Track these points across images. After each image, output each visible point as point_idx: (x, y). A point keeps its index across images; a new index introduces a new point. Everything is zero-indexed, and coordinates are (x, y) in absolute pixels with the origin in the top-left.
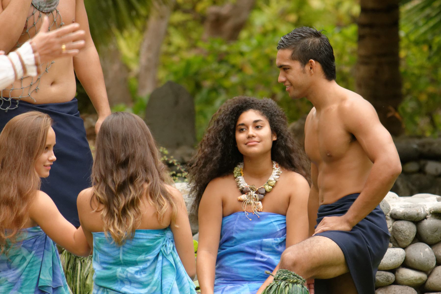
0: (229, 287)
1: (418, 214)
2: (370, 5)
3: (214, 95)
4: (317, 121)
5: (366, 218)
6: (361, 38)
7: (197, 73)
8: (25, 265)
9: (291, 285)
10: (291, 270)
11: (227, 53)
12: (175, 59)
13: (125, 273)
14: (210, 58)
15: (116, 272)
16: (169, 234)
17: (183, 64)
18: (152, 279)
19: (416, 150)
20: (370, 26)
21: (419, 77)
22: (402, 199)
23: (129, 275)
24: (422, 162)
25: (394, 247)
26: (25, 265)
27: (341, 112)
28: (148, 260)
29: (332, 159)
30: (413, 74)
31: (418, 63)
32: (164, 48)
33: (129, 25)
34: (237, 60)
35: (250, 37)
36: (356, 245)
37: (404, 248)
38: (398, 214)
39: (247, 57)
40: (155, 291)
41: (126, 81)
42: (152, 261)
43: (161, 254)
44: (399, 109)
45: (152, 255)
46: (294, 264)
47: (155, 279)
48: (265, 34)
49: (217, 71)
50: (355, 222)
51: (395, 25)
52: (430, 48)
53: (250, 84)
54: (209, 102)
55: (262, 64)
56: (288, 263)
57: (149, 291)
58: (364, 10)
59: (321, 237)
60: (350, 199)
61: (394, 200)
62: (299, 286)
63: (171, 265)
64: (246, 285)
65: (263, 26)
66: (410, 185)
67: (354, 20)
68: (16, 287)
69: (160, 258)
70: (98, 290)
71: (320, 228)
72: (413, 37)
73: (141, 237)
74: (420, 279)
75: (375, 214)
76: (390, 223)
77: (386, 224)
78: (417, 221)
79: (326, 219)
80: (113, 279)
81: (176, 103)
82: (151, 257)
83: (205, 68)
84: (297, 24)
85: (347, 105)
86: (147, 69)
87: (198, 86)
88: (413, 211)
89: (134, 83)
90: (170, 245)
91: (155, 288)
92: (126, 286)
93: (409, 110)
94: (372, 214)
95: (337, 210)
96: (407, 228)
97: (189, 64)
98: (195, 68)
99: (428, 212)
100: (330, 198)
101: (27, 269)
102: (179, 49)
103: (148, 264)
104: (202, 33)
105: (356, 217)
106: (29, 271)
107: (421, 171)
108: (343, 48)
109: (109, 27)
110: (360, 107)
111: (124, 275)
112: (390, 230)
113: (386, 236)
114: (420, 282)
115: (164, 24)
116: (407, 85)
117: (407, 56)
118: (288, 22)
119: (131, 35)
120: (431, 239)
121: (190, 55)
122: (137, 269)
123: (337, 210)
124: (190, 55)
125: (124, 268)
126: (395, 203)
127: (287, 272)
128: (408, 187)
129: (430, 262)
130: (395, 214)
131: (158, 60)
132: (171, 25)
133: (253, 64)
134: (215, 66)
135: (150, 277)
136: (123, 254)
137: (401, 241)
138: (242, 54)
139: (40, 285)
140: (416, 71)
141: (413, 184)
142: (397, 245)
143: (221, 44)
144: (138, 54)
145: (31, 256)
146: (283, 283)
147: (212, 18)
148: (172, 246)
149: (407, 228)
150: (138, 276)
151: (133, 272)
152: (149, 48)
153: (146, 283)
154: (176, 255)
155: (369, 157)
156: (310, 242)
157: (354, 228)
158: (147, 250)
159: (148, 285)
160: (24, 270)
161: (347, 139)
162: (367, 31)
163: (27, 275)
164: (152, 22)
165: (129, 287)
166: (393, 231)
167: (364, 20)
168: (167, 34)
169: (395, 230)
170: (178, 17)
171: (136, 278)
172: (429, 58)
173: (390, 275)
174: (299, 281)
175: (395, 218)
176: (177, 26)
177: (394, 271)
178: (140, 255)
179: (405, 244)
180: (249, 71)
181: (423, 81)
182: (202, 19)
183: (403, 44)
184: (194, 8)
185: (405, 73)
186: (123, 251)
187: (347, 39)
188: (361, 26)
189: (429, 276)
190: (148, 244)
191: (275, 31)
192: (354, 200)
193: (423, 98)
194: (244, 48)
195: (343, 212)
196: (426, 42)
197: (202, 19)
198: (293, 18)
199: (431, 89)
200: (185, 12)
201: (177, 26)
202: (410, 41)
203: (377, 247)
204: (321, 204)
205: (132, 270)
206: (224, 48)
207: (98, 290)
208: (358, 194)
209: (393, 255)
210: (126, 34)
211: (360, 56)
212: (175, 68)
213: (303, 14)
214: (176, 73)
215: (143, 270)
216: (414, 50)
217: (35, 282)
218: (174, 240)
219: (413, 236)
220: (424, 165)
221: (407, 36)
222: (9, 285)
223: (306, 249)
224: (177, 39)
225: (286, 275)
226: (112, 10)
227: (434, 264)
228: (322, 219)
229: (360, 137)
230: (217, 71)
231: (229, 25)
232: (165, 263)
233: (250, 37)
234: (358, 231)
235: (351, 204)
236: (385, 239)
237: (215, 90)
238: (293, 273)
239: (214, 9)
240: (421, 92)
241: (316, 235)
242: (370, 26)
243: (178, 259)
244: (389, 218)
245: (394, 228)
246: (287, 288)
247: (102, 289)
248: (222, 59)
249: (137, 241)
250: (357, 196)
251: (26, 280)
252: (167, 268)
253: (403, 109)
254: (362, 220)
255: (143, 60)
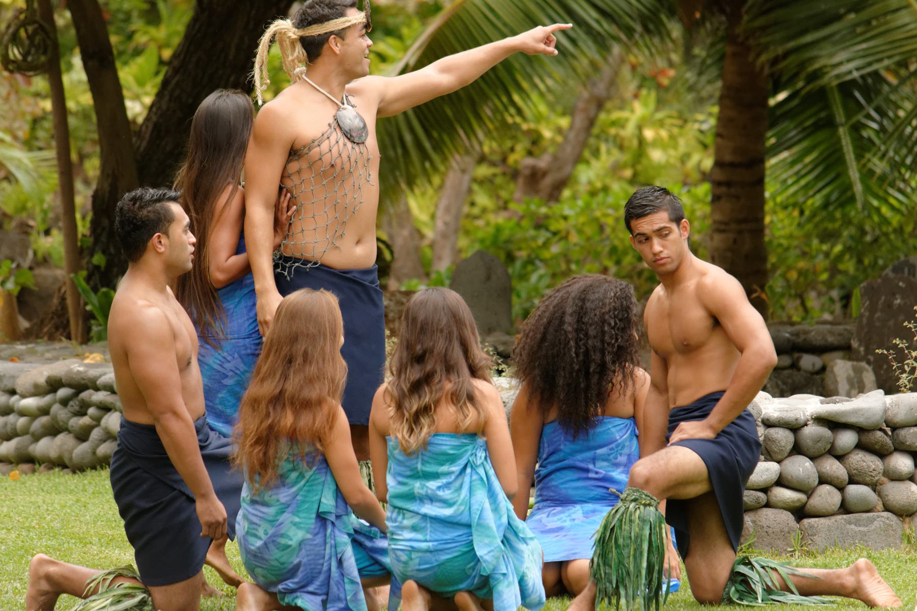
0: (559, 509)
1: (797, 420)
2: (728, 158)
3: (530, 268)
4: (667, 303)
5: (733, 423)
6: (716, 199)
7: (508, 241)
8: (303, 483)
9: (642, 507)
10: (642, 489)
11: (547, 217)
12: (480, 223)
13: (425, 489)
14: (525, 223)
15: (413, 489)
16: (481, 441)
17: (491, 230)
18: (459, 496)
19: (789, 340)
20: (728, 184)
21: (787, 249)
22: (777, 400)
23: (429, 492)
24: (796, 355)
25: (766, 460)
26: (303, 483)
27: (700, 288)
28: (453, 472)
29: (689, 349)
30: (780, 245)
31: (786, 231)
32: (466, 209)
33: (420, 181)
34: (560, 225)
35: (574, 197)
36: (723, 457)
37: (779, 462)
38: (772, 419)
39: (572, 222)
40: (463, 512)
41: (418, 249)
42: (457, 473)
43: (469, 465)
44: (766, 288)
45: (459, 465)
46: (647, 482)
47: (462, 497)
48: (593, 193)
49: (534, 239)
50: (721, 427)
51: (760, 182)
52: (802, 213)
53: (575, 256)
54: (524, 277)
55: (589, 231)
56: (640, 480)
57: (455, 511)
58: (718, 164)
59: (679, 447)
60: (712, 399)
61: (767, 401)
62: (652, 509)
63: (482, 479)
64: (578, 507)
65: (590, 183)
66: (780, 383)
67: (705, 177)
68: (290, 509)
69: (469, 470)
70: (392, 512)
71: (676, 436)
72: (779, 199)
73: (440, 442)
74: (799, 500)
75: (744, 417)
76: (761, 431)
77: (756, 432)
78: (795, 428)
79: (684, 425)
80: (411, 497)
81: (488, 278)
82: (456, 468)
83: (519, 235)
84: (632, 181)
85: (708, 281)
86: (444, 236)
87: (510, 258)
88: (790, 416)
89: (428, 252)
90: (481, 454)
91: (462, 508)
92: (427, 506)
93: (778, 290)
94: (740, 417)
95: (696, 414)
96: (783, 437)
97: (498, 229)
98: (505, 234)
99: (809, 418)
100: (685, 399)
101: (306, 488)
102: (484, 210)
103: (453, 477)
104: (514, 191)
105: (721, 421)
106: (308, 491)
107: (795, 366)
108: (693, 211)
109: (397, 183)
110: (725, 285)
111: (423, 492)
112: (761, 439)
113: (758, 444)
114: (798, 504)
115: (466, 178)
116: (772, 259)
117: (772, 222)
118: (621, 178)
119: (424, 194)
120: (812, 452)
121: (500, 219)
122: (440, 484)
123: (696, 414)
124: (500, 219)
125: (423, 483)
126: (768, 405)
127: (638, 491)
128: (778, 386)
129: (811, 480)
130: (768, 420)
131: (459, 225)
132: (475, 180)
133: (580, 232)
134: (532, 232)
135: (456, 494)
136: (422, 464)
137: (775, 452)
138: (565, 218)
139: (321, 510)
140: (785, 242)
141: (784, 383)
142: (770, 457)
143: (539, 206)
144: (433, 217)
145: (311, 473)
146: (632, 505)
147: (527, 172)
148: (484, 455)
149: (783, 437)
150: (440, 493)
151: (434, 488)
152: (447, 210)
153: (451, 501)
154: (489, 467)
155: (736, 345)
156: (666, 453)
157: (718, 435)
158: (452, 459)
159: (454, 504)
160: (300, 489)
161: (708, 323)
162: (723, 189)
163: (305, 496)
164: (452, 177)
165: (430, 506)
166: (764, 440)
167: (719, 176)
168: (470, 191)
169: (767, 438)
170: (483, 171)
171: (437, 495)
172: (800, 225)
173: (761, 495)
174: (653, 502)
175: (768, 424)
176: (481, 182)
177: (765, 490)
178: (442, 465)
179: (780, 457)
180: (574, 238)
181: (793, 253)
182: (514, 175)
183: (769, 206)
184: (504, 160)
185: (770, 242)
186: (422, 460)
187: (697, 200)
188: (717, 184)
189: (808, 498)
190: (451, 452)
191: (605, 189)
192: (717, 400)
193: (793, 275)
194: (567, 211)
195: (704, 416)
196: (795, 205)
197: (514, 175)
198: (628, 173)
199: (802, 264)
200: (493, 164)
201: (481, 182)
202: (776, 204)
203: (748, 459)
204: (672, 406)
205: (433, 485)
206: (544, 210)
207: (392, 512)
208: (724, 391)
209: (765, 470)
210: (417, 191)
211: (715, 222)
212: (480, 234)
213: (639, 168)
214: (482, 241)
215: (447, 486)
216: (782, 215)
217: (316, 506)
218: (487, 448)
219: (790, 447)
220: (799, 359)
221: (773, 197)
222: (282, 506)
223: (662, 462)
224: (483, 199)
225: (636, 495)
226: (401, 160)
227: (816, 483)
228: (677, 425)
229: (725, 321)
230: (534, 239)
231: (547, 182)
232: (475, 477)
233: (574, 197)
234: (723, 439)
235: (714, 406)
236: (758, 450)
237: (530, 262)
238: (645, 492)
239: (529, 161)
240: (789, 268)
241: (672, 444)
242: (728, 184)
243: (491, 472)
244: (760, 424)
245: (766, 437)
246: (638, 512)
247: (396, 510)
248: (540, 224)
249: (439, 447)
250: (722, 395)
251: (304, 502)
252: (477, 483)
253: (771, 287)
254: (729, 426)
255: (440, 224)
